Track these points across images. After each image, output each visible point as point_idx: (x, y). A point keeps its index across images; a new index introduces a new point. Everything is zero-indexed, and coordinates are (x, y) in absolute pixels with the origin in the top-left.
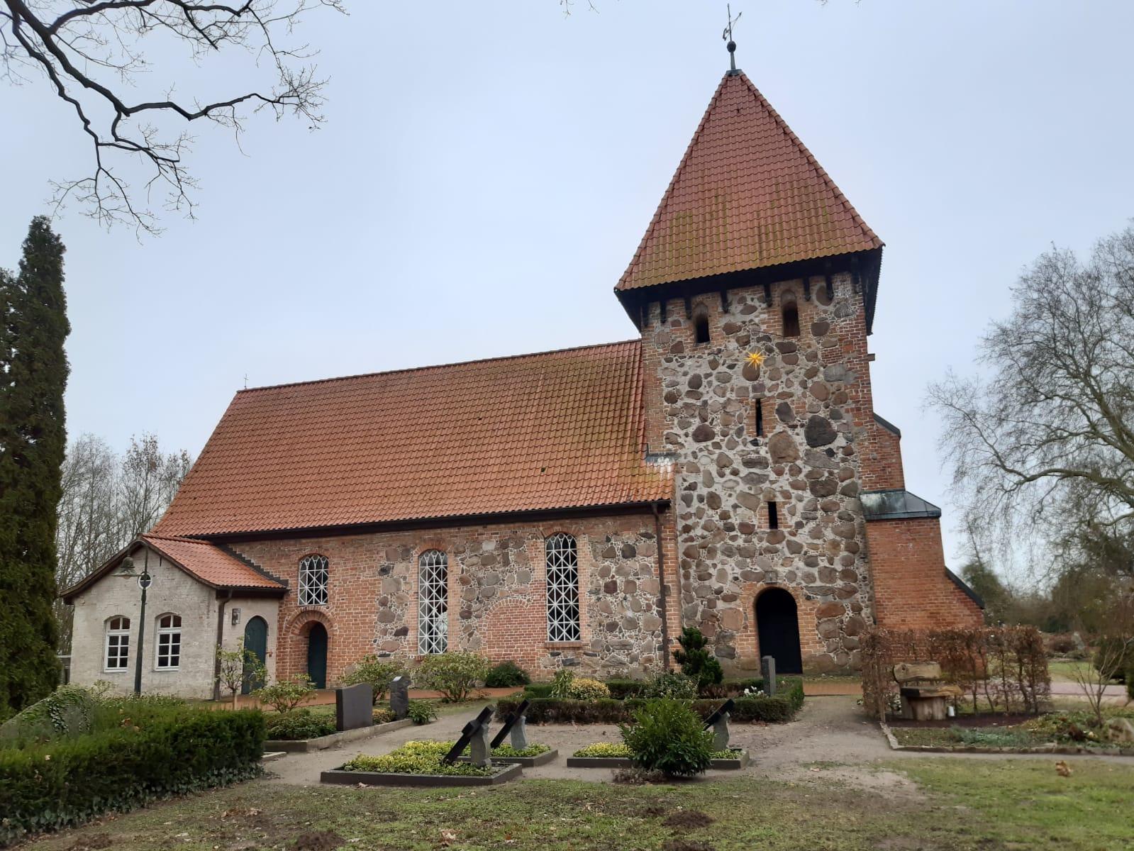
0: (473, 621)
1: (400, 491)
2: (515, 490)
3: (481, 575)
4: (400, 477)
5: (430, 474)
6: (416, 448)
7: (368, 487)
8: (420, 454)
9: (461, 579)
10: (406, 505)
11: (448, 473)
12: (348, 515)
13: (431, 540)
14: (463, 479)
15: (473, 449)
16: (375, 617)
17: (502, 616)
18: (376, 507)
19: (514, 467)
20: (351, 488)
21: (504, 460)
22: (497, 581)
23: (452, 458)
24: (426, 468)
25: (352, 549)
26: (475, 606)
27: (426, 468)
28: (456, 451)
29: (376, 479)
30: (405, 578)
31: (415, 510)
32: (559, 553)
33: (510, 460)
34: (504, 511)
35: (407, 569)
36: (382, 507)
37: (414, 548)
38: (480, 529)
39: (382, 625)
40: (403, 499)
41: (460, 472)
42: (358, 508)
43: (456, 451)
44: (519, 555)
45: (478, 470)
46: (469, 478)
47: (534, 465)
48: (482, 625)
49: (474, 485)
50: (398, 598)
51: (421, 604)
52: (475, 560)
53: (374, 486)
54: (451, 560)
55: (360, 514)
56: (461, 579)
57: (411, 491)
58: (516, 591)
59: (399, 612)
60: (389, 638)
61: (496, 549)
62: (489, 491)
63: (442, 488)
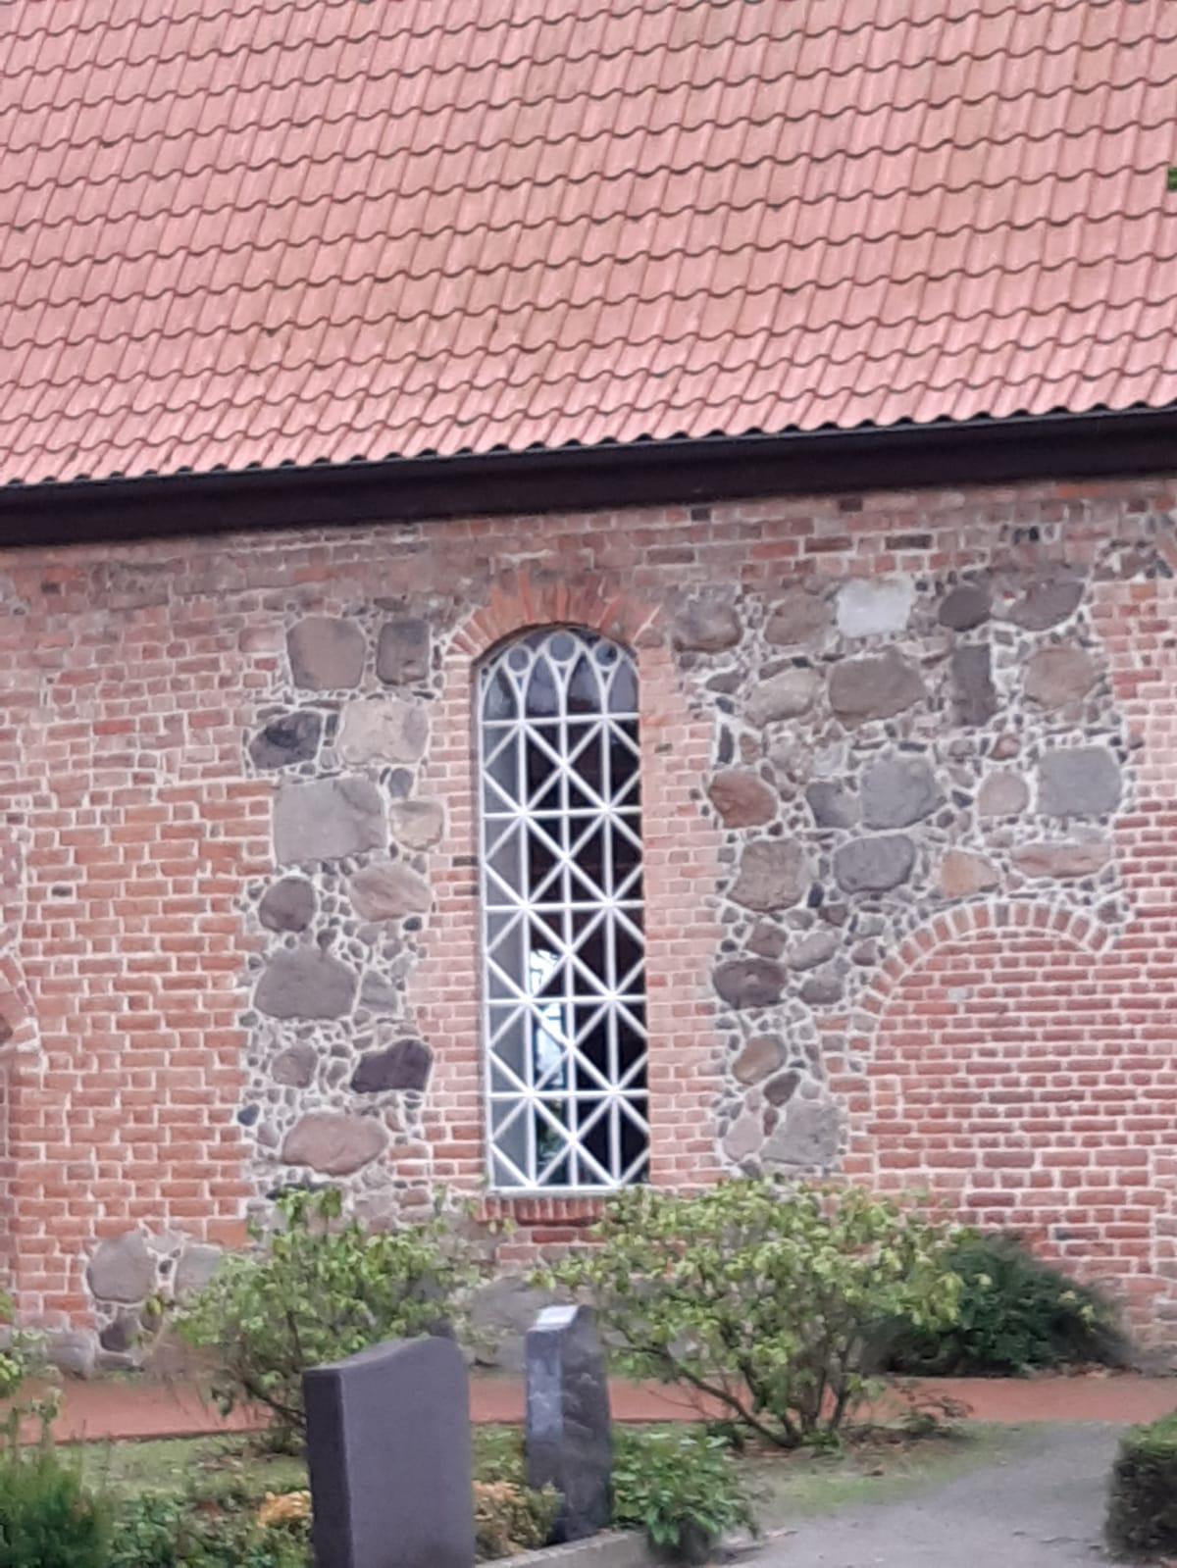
0: (793, 1020)
1: (347, 302)
2: (1018, 293)
3: (830, 768)
4: (339, 220)
5: (507, 208)
6: (419, 53)
7: (161, 276)
8: (442, 90)
9: (717, 789)
10: (393, 377)
11: (612, 198)
12: (68, 433)
13: (543, 573)
14: (704, 232)
15: (752, 56)
16: (240, 988)
17: (956, 995)
18: (220, 390)
19: (1001, 163)
20: (65, 283)
21: (940, 125)
22: (923, 801)
23: (632, 114)
24: (485, 167)
25: (99, 619)
26: (798, 939)
27: (485, 167)
28: (646, 71)
29: (206, 232)
30: (400, 781)
31: (445, 406)
32: (550, 734)
33: (974, 123)
34: (963, 414)
35: (413, 733)
36: (252, 387)
37: (445, 619)
38: (822, 515)
39: (286, 1034)
40: (370, 343)
41: (682, 193)
42: (117, 396)
43: (646, 71)
44: (1046, 660)
45: (790, 181)
46: (742, 228)
47: (1120, 150)
48: (848, 1040)
49: (770, 269)
50: (366, 886)
51: (497, 921)
52: (794, 686)
53: (195, 272)
54: (661, 687)
55: (136, 428)
56: (717, 789)
57: (413, 299)
58: (1034, 860)
59: (377, 965)
60: (323, 1099)
61: (916, 628)
62: (864, 306)
63: (588, 285)
